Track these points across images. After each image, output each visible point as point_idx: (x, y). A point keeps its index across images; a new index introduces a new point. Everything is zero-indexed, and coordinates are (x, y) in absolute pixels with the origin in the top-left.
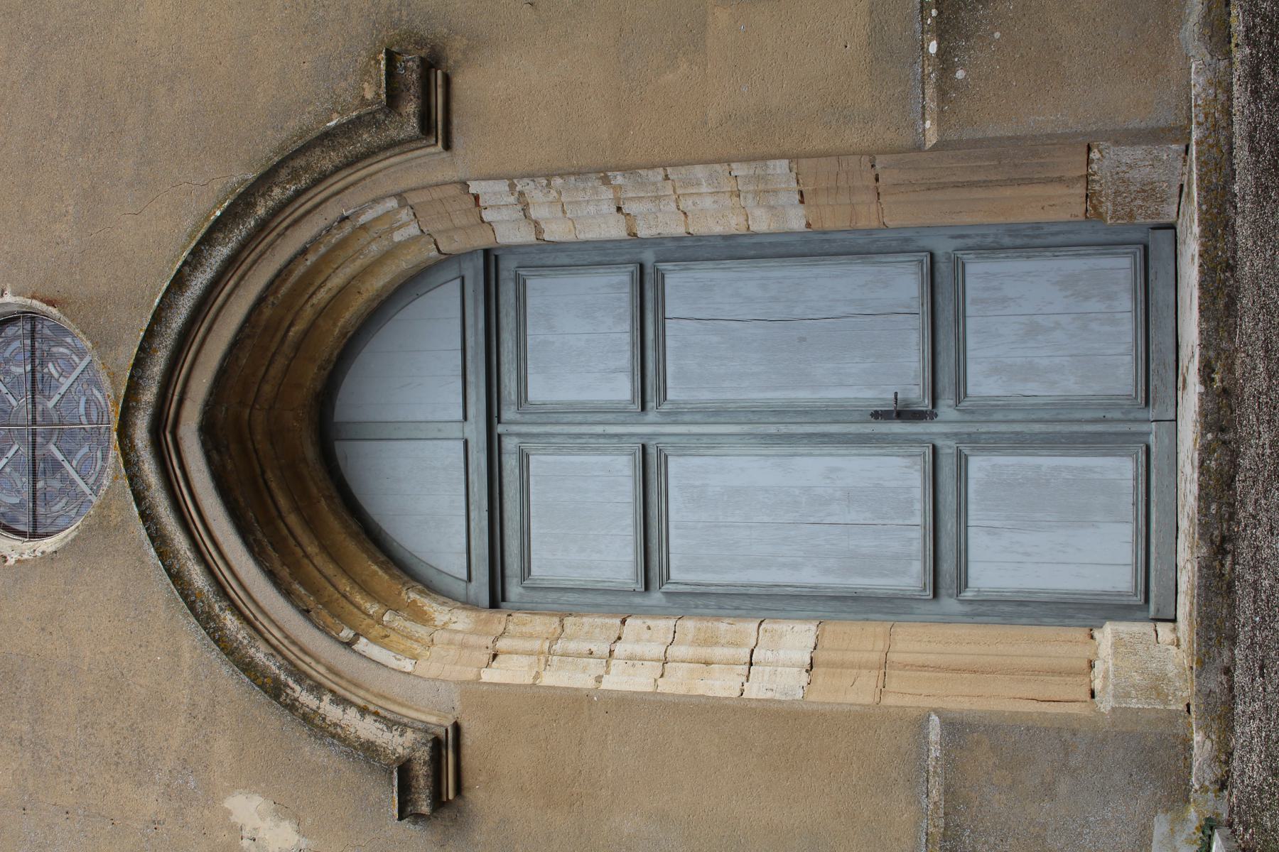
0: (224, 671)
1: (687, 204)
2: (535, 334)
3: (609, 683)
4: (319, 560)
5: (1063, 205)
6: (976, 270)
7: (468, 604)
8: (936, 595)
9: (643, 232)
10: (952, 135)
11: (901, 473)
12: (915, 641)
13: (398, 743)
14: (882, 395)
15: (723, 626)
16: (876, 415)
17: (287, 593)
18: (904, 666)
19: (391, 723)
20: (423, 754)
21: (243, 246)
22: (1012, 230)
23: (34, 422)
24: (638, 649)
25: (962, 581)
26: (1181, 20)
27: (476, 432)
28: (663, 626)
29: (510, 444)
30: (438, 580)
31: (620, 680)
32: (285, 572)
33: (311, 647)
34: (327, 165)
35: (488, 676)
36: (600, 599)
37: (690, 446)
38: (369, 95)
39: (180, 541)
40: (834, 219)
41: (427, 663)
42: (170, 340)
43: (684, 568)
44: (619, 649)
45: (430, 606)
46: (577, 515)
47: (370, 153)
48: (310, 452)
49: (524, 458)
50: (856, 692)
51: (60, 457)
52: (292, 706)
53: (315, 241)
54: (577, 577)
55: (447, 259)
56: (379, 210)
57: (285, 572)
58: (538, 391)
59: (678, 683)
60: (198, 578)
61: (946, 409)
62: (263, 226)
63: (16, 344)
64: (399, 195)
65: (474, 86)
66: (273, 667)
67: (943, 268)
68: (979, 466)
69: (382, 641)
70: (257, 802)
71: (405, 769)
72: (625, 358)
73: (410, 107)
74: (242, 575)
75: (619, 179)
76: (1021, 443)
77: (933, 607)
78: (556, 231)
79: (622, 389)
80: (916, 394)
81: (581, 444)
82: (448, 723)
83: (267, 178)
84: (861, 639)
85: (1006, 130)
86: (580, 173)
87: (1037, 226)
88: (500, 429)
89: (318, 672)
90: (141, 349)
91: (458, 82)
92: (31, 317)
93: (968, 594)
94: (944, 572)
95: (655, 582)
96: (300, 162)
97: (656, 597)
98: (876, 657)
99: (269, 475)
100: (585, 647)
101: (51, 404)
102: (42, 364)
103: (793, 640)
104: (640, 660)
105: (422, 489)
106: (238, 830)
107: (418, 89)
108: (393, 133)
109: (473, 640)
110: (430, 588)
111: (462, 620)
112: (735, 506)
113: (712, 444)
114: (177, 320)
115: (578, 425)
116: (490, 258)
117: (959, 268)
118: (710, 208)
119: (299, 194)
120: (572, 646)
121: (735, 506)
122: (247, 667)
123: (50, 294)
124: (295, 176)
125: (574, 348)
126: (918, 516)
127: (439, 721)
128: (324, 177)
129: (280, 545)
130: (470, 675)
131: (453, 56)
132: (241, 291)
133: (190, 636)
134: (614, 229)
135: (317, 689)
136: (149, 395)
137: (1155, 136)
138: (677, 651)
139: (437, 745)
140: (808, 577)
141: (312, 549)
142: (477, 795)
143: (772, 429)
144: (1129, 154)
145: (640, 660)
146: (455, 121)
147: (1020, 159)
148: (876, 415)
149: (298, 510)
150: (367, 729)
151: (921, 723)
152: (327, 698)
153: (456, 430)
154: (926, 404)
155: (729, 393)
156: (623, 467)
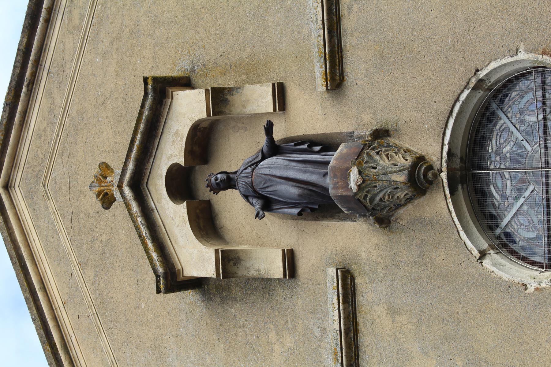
92: (541, 70)
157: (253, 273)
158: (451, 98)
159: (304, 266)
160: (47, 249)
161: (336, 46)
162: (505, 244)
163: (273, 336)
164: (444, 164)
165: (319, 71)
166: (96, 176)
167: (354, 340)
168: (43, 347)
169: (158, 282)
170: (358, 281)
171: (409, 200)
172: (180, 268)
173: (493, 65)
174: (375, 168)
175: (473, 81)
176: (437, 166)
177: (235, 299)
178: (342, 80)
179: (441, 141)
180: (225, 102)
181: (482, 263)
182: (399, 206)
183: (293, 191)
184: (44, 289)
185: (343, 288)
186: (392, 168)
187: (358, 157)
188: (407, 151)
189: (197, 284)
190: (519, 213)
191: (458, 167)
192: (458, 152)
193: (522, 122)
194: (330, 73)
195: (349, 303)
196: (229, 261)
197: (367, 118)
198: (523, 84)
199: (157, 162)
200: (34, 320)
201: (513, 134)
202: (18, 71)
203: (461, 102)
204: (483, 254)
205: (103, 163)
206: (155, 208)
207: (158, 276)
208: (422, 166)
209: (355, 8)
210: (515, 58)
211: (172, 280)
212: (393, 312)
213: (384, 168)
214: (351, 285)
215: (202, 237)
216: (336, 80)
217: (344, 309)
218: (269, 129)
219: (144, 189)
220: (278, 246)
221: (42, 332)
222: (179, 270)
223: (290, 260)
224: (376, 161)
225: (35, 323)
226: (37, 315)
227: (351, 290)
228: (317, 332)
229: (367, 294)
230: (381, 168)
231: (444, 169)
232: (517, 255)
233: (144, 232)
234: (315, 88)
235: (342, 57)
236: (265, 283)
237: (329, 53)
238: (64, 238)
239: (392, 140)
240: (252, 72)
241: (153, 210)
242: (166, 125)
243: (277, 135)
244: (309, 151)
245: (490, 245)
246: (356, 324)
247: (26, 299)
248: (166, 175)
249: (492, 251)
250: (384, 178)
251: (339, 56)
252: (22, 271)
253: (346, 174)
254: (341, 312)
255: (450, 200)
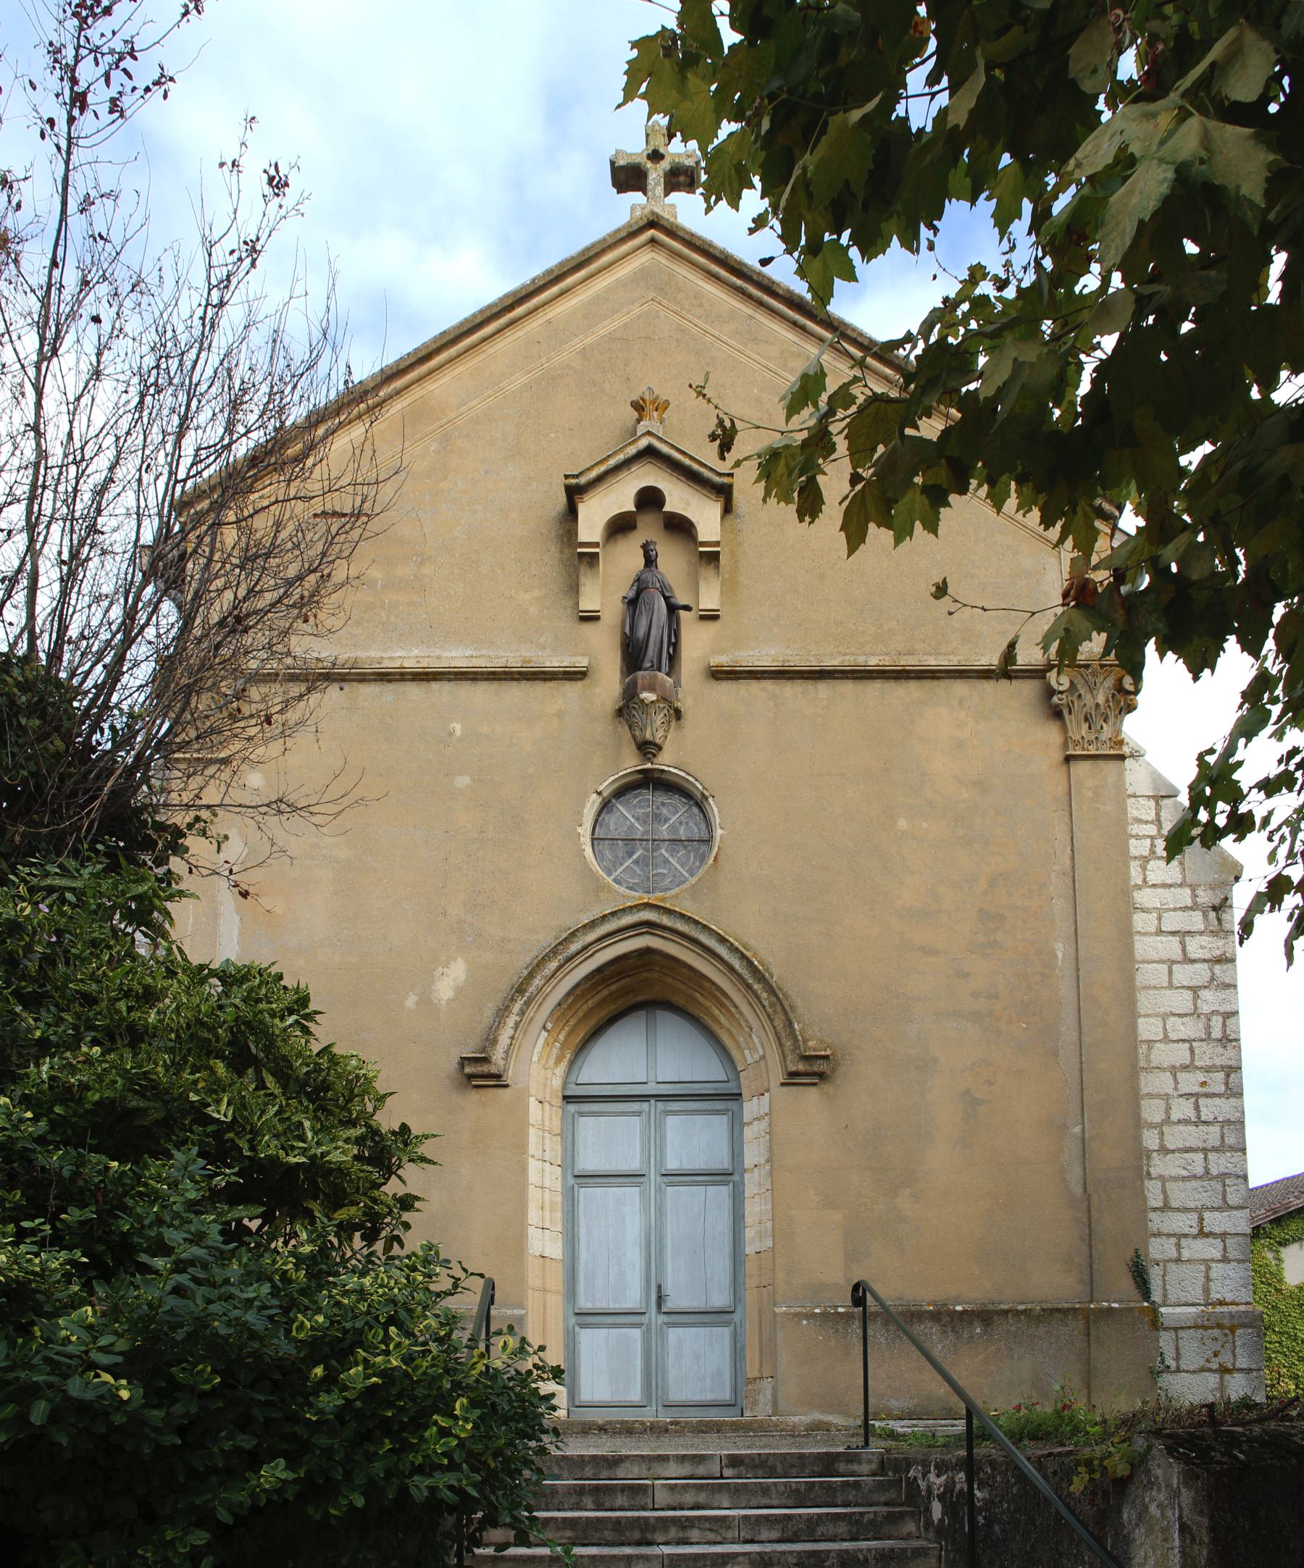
0: (527, 959)
1: (757, 1199)
2: (699, 1119)
3: (532, 1162)
4: (585, 1008)
5: (752, 1370)
6: (726, 1332)
7: (565, 1084)
8: (577, 1314)
9: (746, 1176)
10: (778, 1319)
11: (633, 1297)
12: (556, 1304)
13: (498, 1055)
14: (669, 1289)
15: (559, 1215)
16: (659, 1287)
17: (569, 994)
18: (545, 1299)
19: (507, 1052)
20: (494, 1070)
21: (739, 975)
22: (743, 1348)
23: (654, 840)
24: (547, 1174)
25: (583, 1326)
26: (822, 1412)
27: (651, 1089)
28: (558, 1185)
29: (645, 1106)
30: (576, 1066)
31: (533, 1166)
32: (578, 992)
33: (542, 1008)
34: (777, 1023)
35: (532, 1100)
36: (569, 1153)
37: (645, 1198)
38: (810, 1044)
39: (592, 936)
40: (751, 1267)
41: (536, 1066)
42: (693, 933)
43: (587, 1195)
44: (547, 1164)
45: (563, 1066)
46: (611, 1140)
47: (781, 1045)
48: (640, 998)
49: (638, 1114)
50: (533, 1278)
51: (635, 857)
52: (513, 1000)
53: (741, 1013)
54: (580, 1140)
55: (738, 1073)
56: (758, 1045)
57: (578, 992)
58: (671, 1121)
59: (534, 1195)
60: (574, 947)
61: (662, 1318)
62: (749, 987)
63: (696, 830)
64: (763, 1057)
65: (811, 1096)
66: (532, 989)
67: (727, 1317)
68: (636, 1333)
69: (547, 1043)
70: (463, 977)
71: (485, 1060)
72: (687, 1166)
73: (801, 1067)
74: (577, 970)
75: (768, 1168)
76: (647, 1352)
77: (571, 1312)
78: (748, 1133)
79: (672, 1164)
80: (669, 1305)
81: (646, 1143)
82: (508, 1082)
83: (771, 990)
84: (556, 1280)
85: (779, 1341)
86: (770, 1149)
87: (744, 1359)
88: (653, 1101)
89: (530, 1013)
90: (690, 918)
91: (813, 1089)
92: (708, 841)
93: (577, 1329)
94: (587, 1318)
95: (579, 1181)
96: (779, 1009)
97: (571, 1181)
98: (548, 1286)
99: (628, 980)
100: (547, 1148)
101: (663, 851)
102: (685, 847)
103: (554, 1249)
104: (543, 1176)
105: (623, 1058)
106: (446, 965)
107: (812, 1070)
108: (789, 1058)
109: (548, 1090)
110: (572, 1063)
111: (557, 1082)
112: (617, 1220)
113: (646, 1209)
114: (703, 938)
115: (655, 1142)
116: (737, 1096)
117: (727, 1324)
118: (755, 1209)
119: (764, 1007)
120: (547, 1141)
121: (617, 1220)
122: (531, 976)
123: (721, 858)
124: (772, 1005)
125: (693, 1139)
126: (613, 1306)
127: (509, 1078)
128: (772, 1021)
129: (593, 986)
130: (532, 1091)
131: (826, 1087)
132: (718, 973)
133: (545, 939)
134: (748, 1163)
135: (522, 1013)
136: (666, 920)
137: (775, 1403)
138: (547, 1195)
139: (498, 1077)
140: (583, 1255)
141: (590, 1003)
142: (474, 1096)
143: (653, 1238)
144: (769, 1393)
145: (543, 1176)
146: (794, 1088)
147: (768, 1350)
148: (659, 1287)
149: (610, 994)
150: (504, 1040)
151: (521, 1306)
152: (518, 1018)
153: (652, 1078)
154: (664, 1309)
155: (670, 1217)
156: (634, 1165)
157: (582, 580)
158: (698, 775)
159: (588, 628)
160: (597, 299)
162: (606, 806)
163: (536, 593)
165: (722, 660)
166: (658, 397)
169: (574, 476)
170: (580, 683)
171: (634, 737)
173: (715, 809)
175: (707, 793)
176: (655, 760)
177: (562, 552)
178: (717, 679)
180: (709, 562)
182: (630, 727)
183: (641, 632)
184: (562, 293)
186: (655, 728)
189: (571, 512)
190: (627, 815)
192: (663, 776)
193: (681, 823)
197: (689, 701)
198: (703, 826)
199: (667, 476)
201: (676, 816)
202: (755, 277)
204: (599, 793)
207: (577, 476)
209: (764, 694)
211: (575, 493)
212: (560, 715)
216: (719, 674)
218: (687, 608)
220: (602, 604)
221: (524, 293)
223: (590, 618)
228: (542, 640)
229: (571, 690)
232: (599, 815)
233: (612, 462)
234: (714, 653)
236: (574, 589)
238: (604, 328)
239: (673, 723)
240: (729, 590)
243: (682, 613)
244: (669, 643)
246: (550, 680)
253: (651, 689)
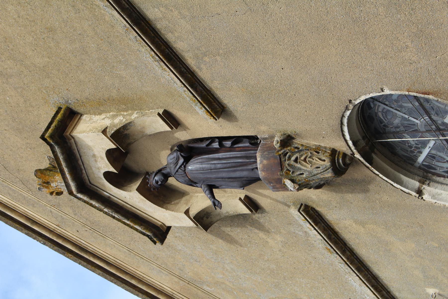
161: (203, 91)
164: (353, 148)
167: (337, 238)
168: (65, 256)
172: (160, 223)
174: (303, 174)
176: (349, 152)
179: (343, 140)
180: (127, 136)
181: (422, 198)
185: (310, 218)
187: (281, 167)
188: (318, 150)
191: (364, 144)
194: (212, 111)
195: (319, 223)
196: (202, 219)
200: (44, 244)
203: (347, 117)
204: (420, 192)
205: (36, 171)
206: (109, 195)
208: (338, 159)
210: (383, 93)
213: (310, 173)
214: (314, 213)
215: (164, 203)
217: (319, 228)
219: (90, 186)
221: (56, 248)
222: (161, 225)
224: (300, 169)
225: (47, 245)
226: (43, 240)
227: (317, 215)
230: (307, 173)
231: (355, 151)
235: (213, 95)
237: (202, 99)
241: (109, 197)
242: (80, 152)
245: (420, 181)
247: (26, 234)
248: (105, 177)
249: (424, 186)
250: (314, 178)
251: (210, 96)
252: (7, 219)
254: (318, 230)
255: (372, 168)
